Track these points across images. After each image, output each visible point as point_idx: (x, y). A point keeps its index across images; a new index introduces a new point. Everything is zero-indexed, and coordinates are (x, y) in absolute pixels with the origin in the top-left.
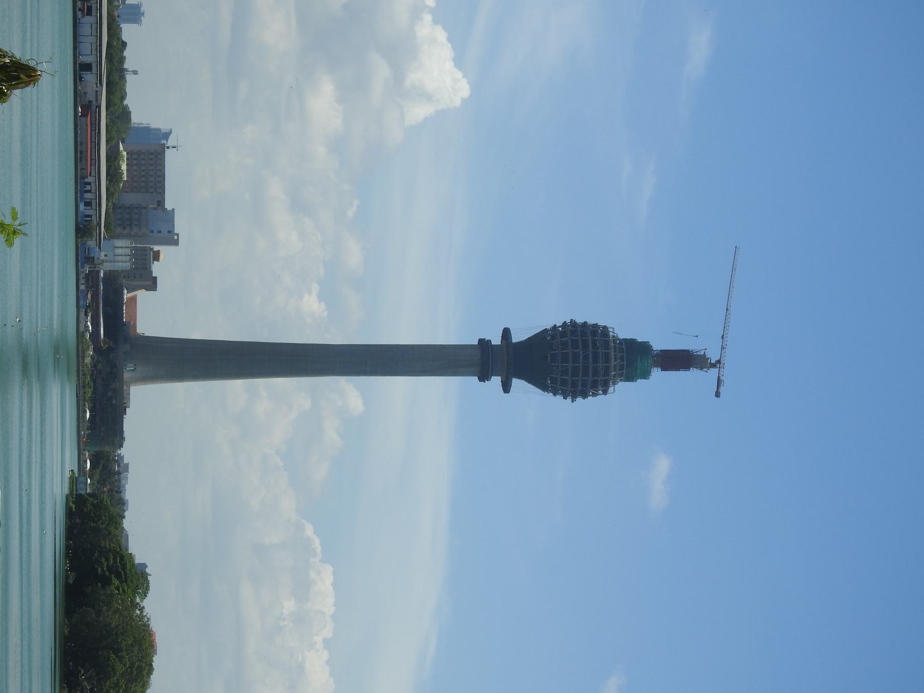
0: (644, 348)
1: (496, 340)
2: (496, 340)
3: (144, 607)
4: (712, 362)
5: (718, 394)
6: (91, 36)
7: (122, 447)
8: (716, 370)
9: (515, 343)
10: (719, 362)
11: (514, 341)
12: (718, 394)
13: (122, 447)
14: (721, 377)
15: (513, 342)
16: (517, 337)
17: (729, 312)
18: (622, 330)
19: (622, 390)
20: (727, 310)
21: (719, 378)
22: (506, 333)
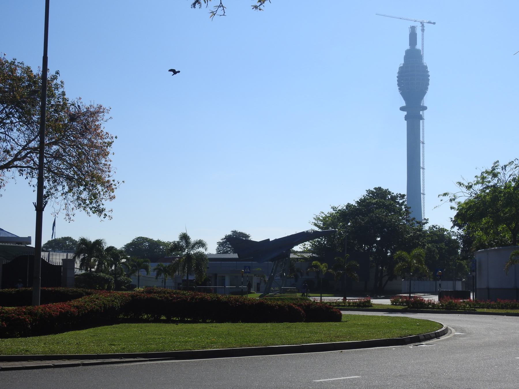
0: (407, 52)
1: (405, 113)
2: (405, 113)
3: (433, 225)
4: (68, 258)
5: (434, 23)
6: (224, 15)
7: (269, 239)
8: (424, 24)
9: (406, 103)
10: (421, 23)
11: (405, 105)
12: (434, 23)
13: (269, 239)
14: (427, 22)
15: (405, 105)
16: (404, 104)
17: (402, 18)
18: (400, 61)
19: (427, 60)
20: (401, 19)
21: (427, 23)
22: (402, 109)
